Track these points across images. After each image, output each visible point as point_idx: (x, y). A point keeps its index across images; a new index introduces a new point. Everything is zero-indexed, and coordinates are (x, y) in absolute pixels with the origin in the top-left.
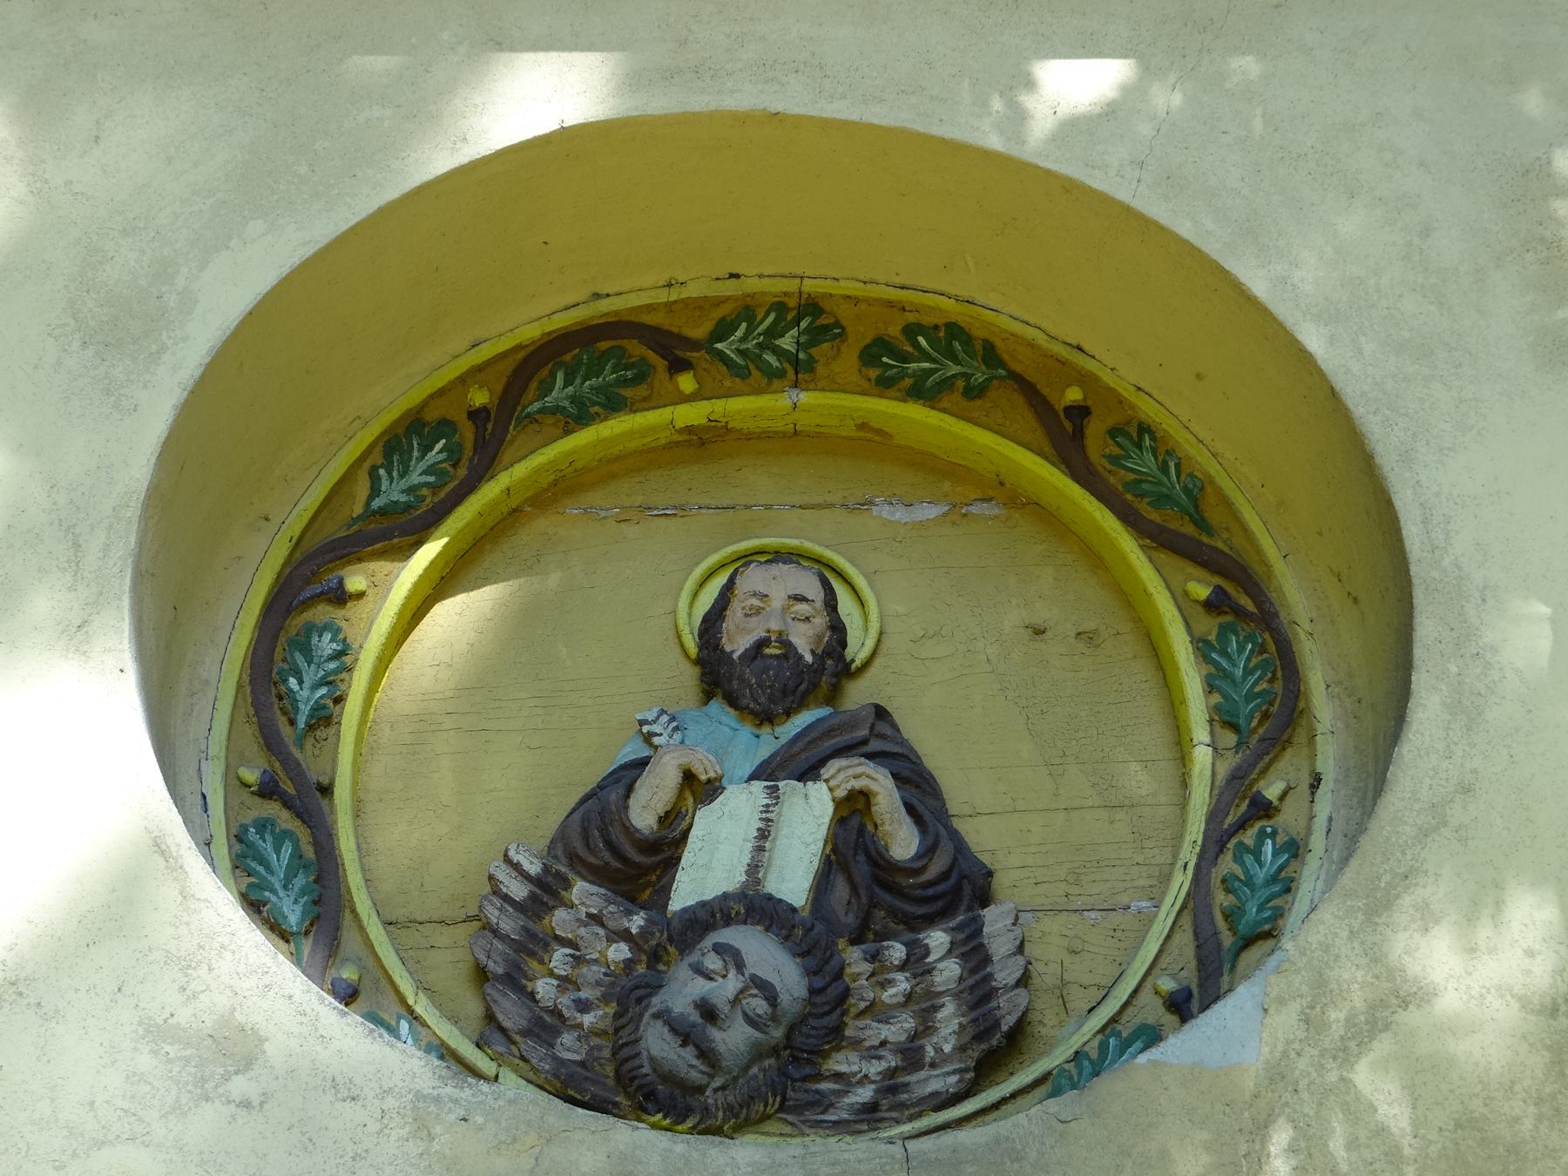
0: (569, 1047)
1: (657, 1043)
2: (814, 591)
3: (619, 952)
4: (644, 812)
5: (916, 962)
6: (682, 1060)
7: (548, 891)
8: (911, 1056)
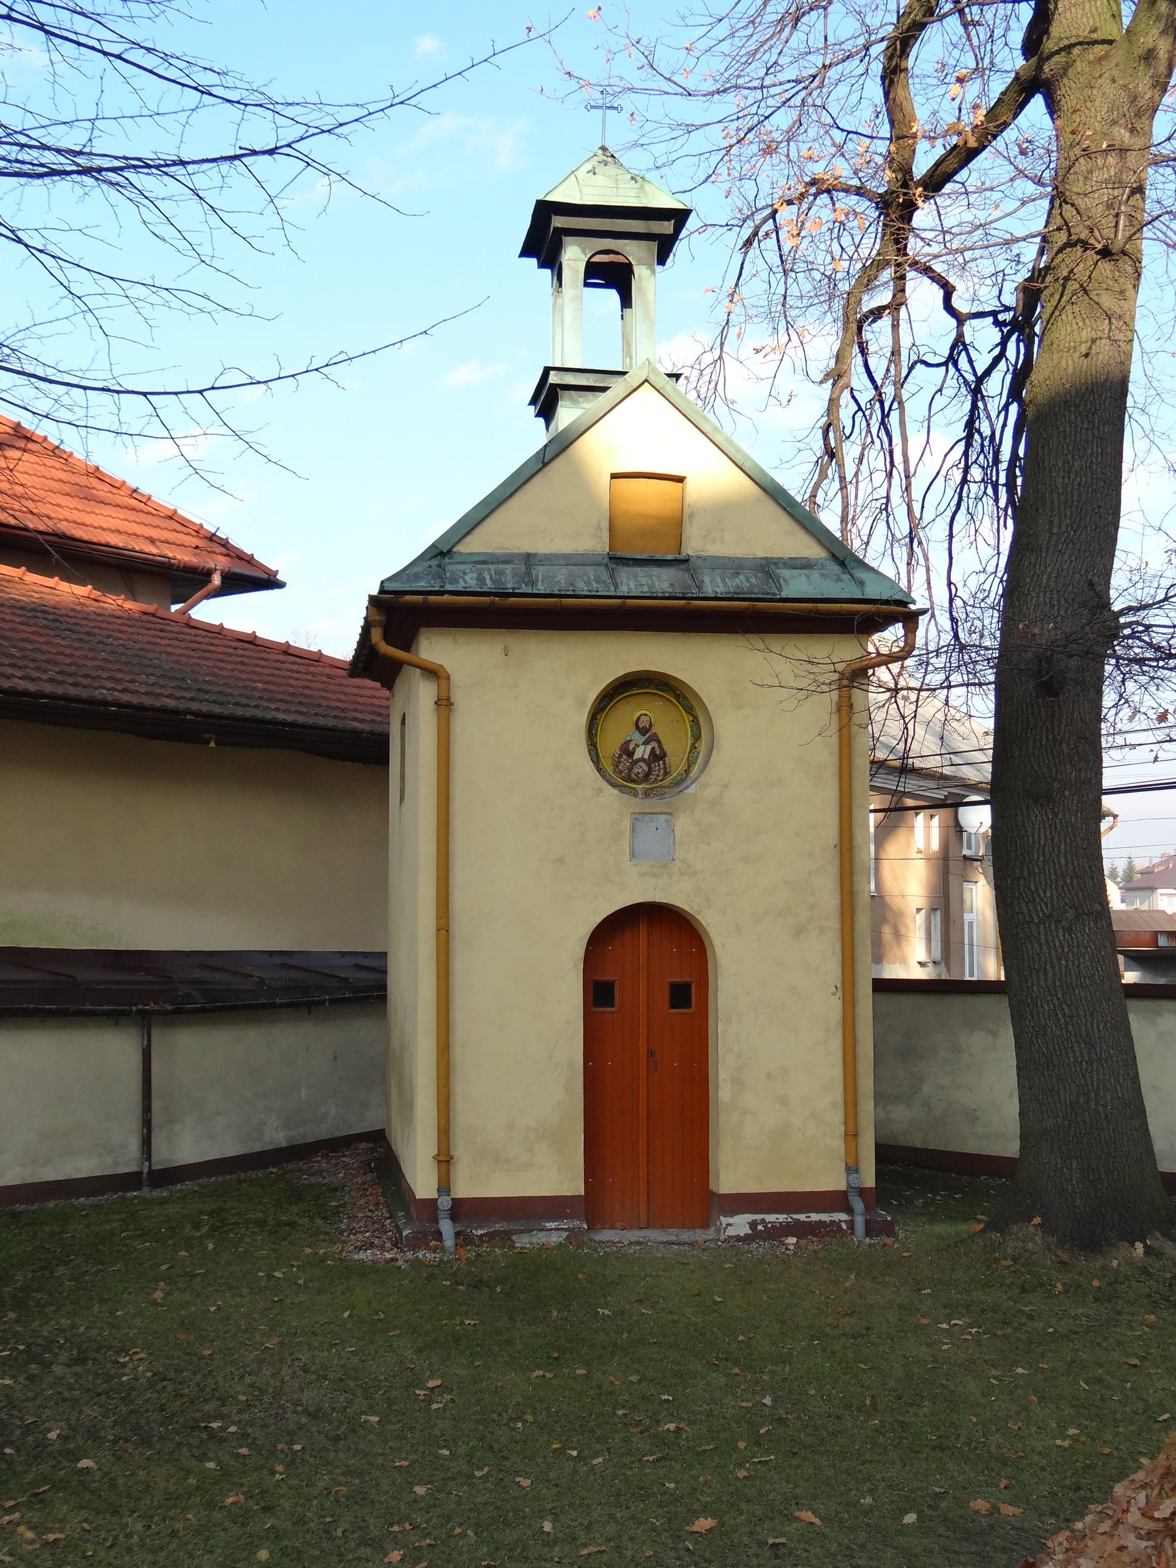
1: (634, 777)
5: (659, 765)
8: (658, 776)
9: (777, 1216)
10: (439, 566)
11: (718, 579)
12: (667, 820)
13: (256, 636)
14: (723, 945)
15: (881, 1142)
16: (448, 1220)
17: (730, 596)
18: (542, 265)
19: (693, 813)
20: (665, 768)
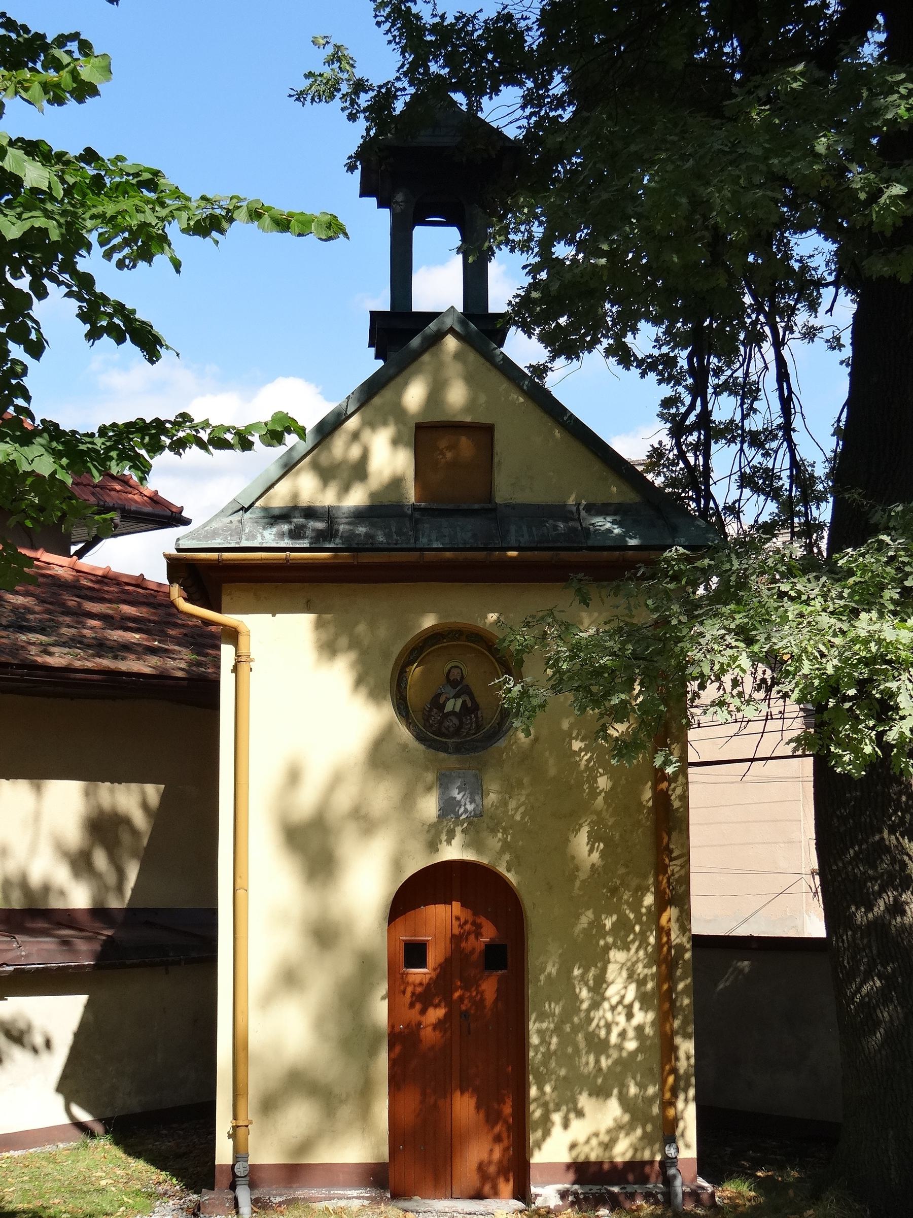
0: (434, 729)
1: (443, 730)
2: (460, 671)
3: (439, 718)
4: (442, 700)
5: (471, 717)
6: (446, 732)
7: (431, 710)
8: (470, 729)
9: (590, 1187)
10: (240, 522)
11: (525, 529)
12: (476, 776)
13: (144, 579)
14: (534, 904)
15: (108, 1114)
16: (247, 1187)
17: (533, 545)
18: (381, 205)
19: (502, 768)
20: (477, 721)
